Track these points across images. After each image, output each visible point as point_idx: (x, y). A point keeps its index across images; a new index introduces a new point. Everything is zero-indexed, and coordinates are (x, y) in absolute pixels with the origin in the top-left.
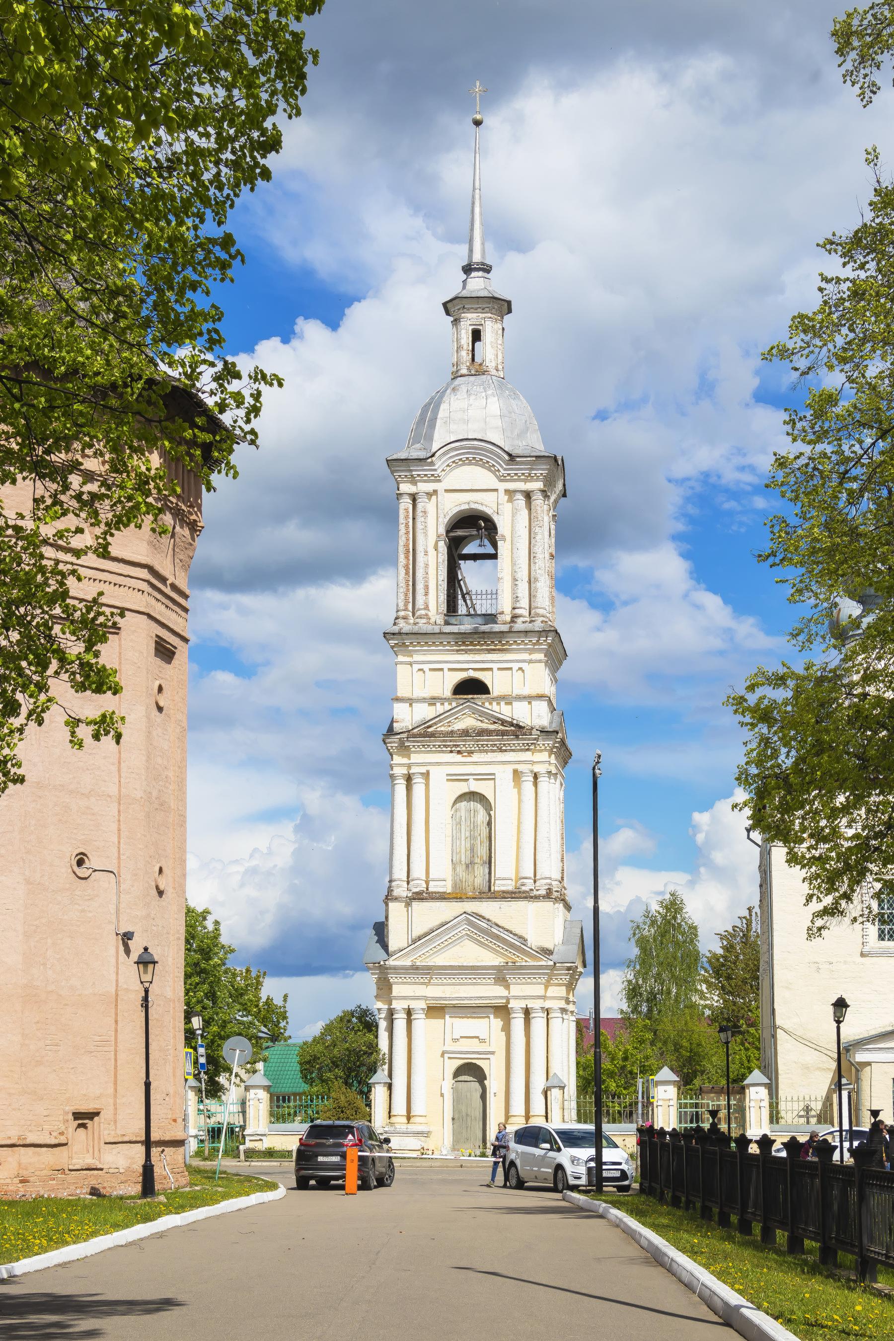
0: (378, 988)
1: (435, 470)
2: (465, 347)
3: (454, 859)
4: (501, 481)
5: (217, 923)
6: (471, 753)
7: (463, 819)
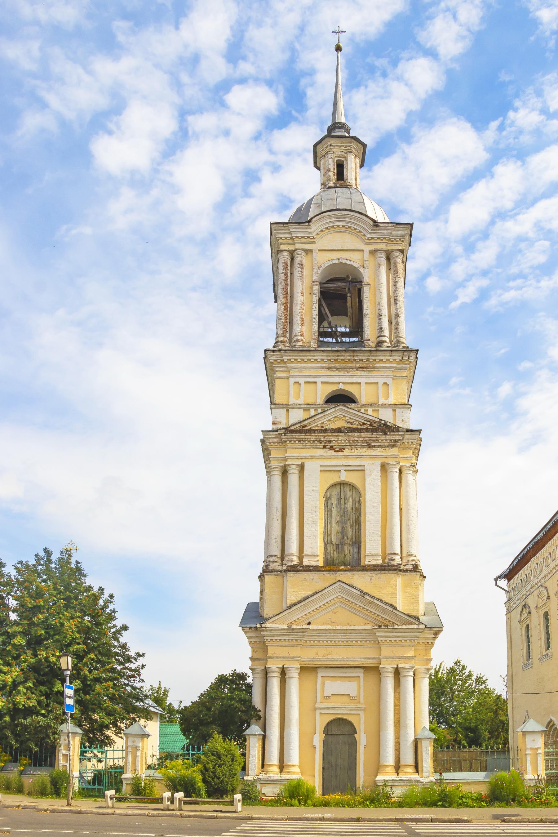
0: (253, 651)
1: (311, 233)
2: (332, 170)
3: (326, 540)
4: (367, 243)
5: (77, 562)
6: (342, 450)
7: (334, 506)
